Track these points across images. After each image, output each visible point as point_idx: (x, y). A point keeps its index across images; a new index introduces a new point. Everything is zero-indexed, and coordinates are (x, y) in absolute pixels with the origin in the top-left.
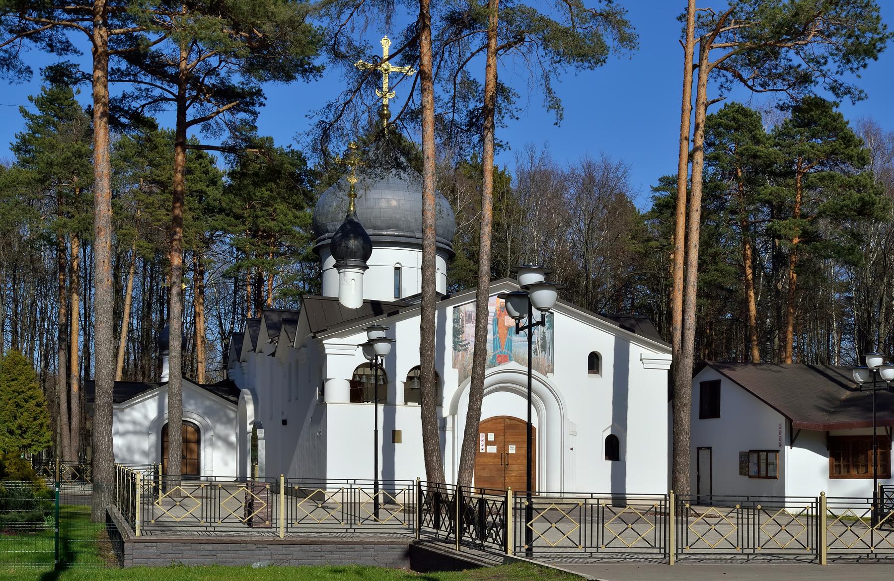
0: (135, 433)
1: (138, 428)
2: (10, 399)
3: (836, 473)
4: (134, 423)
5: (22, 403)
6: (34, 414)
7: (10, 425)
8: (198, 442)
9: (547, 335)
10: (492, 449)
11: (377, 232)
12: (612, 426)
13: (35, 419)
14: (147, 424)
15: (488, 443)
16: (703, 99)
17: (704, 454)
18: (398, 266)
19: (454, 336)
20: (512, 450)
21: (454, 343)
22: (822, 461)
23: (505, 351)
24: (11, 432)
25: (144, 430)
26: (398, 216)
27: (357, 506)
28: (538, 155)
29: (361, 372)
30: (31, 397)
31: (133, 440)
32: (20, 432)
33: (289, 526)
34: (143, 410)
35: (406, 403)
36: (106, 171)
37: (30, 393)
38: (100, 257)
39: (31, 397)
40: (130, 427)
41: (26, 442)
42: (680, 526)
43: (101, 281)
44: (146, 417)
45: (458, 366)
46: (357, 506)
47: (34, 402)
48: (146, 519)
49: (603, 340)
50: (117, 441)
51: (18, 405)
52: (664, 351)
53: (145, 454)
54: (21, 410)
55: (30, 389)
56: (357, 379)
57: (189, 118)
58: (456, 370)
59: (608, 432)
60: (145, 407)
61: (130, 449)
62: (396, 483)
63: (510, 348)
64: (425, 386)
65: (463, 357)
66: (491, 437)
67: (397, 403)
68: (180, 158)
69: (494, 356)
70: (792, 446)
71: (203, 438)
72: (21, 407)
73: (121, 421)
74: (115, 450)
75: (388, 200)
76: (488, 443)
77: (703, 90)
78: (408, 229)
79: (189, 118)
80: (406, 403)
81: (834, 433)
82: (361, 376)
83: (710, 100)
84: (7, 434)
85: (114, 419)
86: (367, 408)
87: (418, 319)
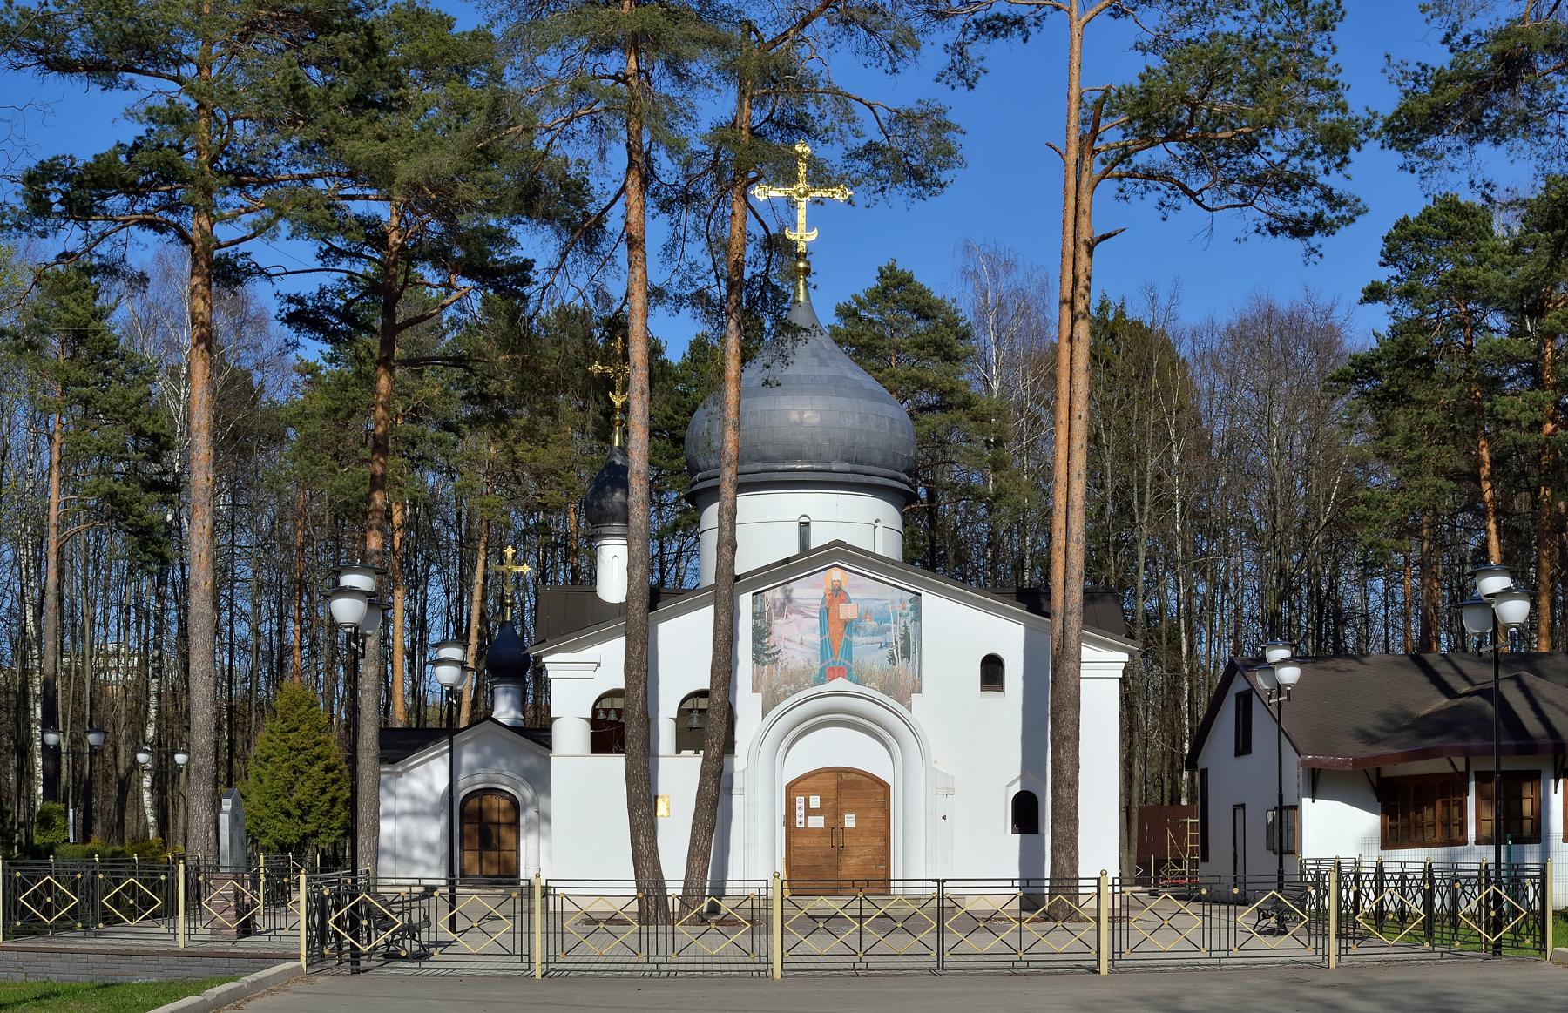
0: (415, 814)
1: (419, 806)
2: (285, 760)
3: (1390, 839)
4: (413, 797)
5: (303, 766)
6: (321, 784)
7: (285, 801)
8: (515, 825)
9: (911, 631)
10: (817, 822)
11: (768, 466)
12: (1023, 777)
13: (323, 791)
14: (432, 799)
15: (809, 812)
16: (1085, 235)
17: (1240, 812)
18: (805, 520)
19: (754, 639)
20: (850, 822)
21: (754, 650)
22: (1368, 822)
23: (841, 660)
24: (288, 814)
25: (428, 809)
26: (801, 438)
27: (558, 917)
28: (1163, 301)
29: (606, 704)
30: (318, 757)
31: (411, 825)
32: (298, 812)
33: (1117, 956)
34: (426, 778)
35: (678, 752)
36: (204, 422)
37: (318, 749)
38: (196, 550)
39: (318, 757)
40: (405, 805)
41: (310, 828)
42: (551, 936)
43: (196, 586)
44: (431, 788)
45: (762, 688)
46: (558, 917)
47: (321, 764)
48: (1117, 949)
49: (1006, 635)
50: (386, 827)
51: (296, 770)
52: (1111, 647)
53: (429, 847)
54: (302, 778)
55: (316, 744)
56: (602, 716)
57: (399, 320)
58: (759, 696)
59: (1017, 788)
60: (429, 771)
61: (407, 841)
62: (667, 884)
63: (849, 656)
64: (710, 724)
65: (771, 673)
66: (815, 802)
67: (661, 753)
68: (383, 382)
69: (822, 670)
70: (1313, 797)
71: (523, 820)
72: (303, 773)
73: (392, 793)
74: (384, 842)
75: (802, 413)
76: (809, 812)
77: (1083, 220)
78: (819, 458)
79: (399, 320)
80: (678, 752)
81: (1390, 771)
82: (607, 711)
83: (1098, 235)
84: (282, 817)
85: (382, 792)
86: (616, 764)
87: (709, 611)
